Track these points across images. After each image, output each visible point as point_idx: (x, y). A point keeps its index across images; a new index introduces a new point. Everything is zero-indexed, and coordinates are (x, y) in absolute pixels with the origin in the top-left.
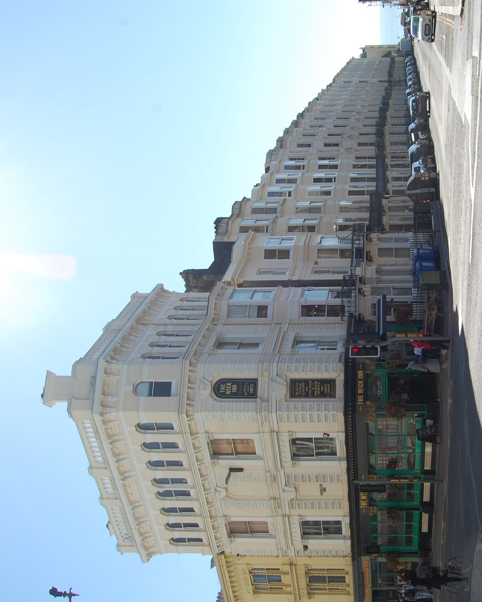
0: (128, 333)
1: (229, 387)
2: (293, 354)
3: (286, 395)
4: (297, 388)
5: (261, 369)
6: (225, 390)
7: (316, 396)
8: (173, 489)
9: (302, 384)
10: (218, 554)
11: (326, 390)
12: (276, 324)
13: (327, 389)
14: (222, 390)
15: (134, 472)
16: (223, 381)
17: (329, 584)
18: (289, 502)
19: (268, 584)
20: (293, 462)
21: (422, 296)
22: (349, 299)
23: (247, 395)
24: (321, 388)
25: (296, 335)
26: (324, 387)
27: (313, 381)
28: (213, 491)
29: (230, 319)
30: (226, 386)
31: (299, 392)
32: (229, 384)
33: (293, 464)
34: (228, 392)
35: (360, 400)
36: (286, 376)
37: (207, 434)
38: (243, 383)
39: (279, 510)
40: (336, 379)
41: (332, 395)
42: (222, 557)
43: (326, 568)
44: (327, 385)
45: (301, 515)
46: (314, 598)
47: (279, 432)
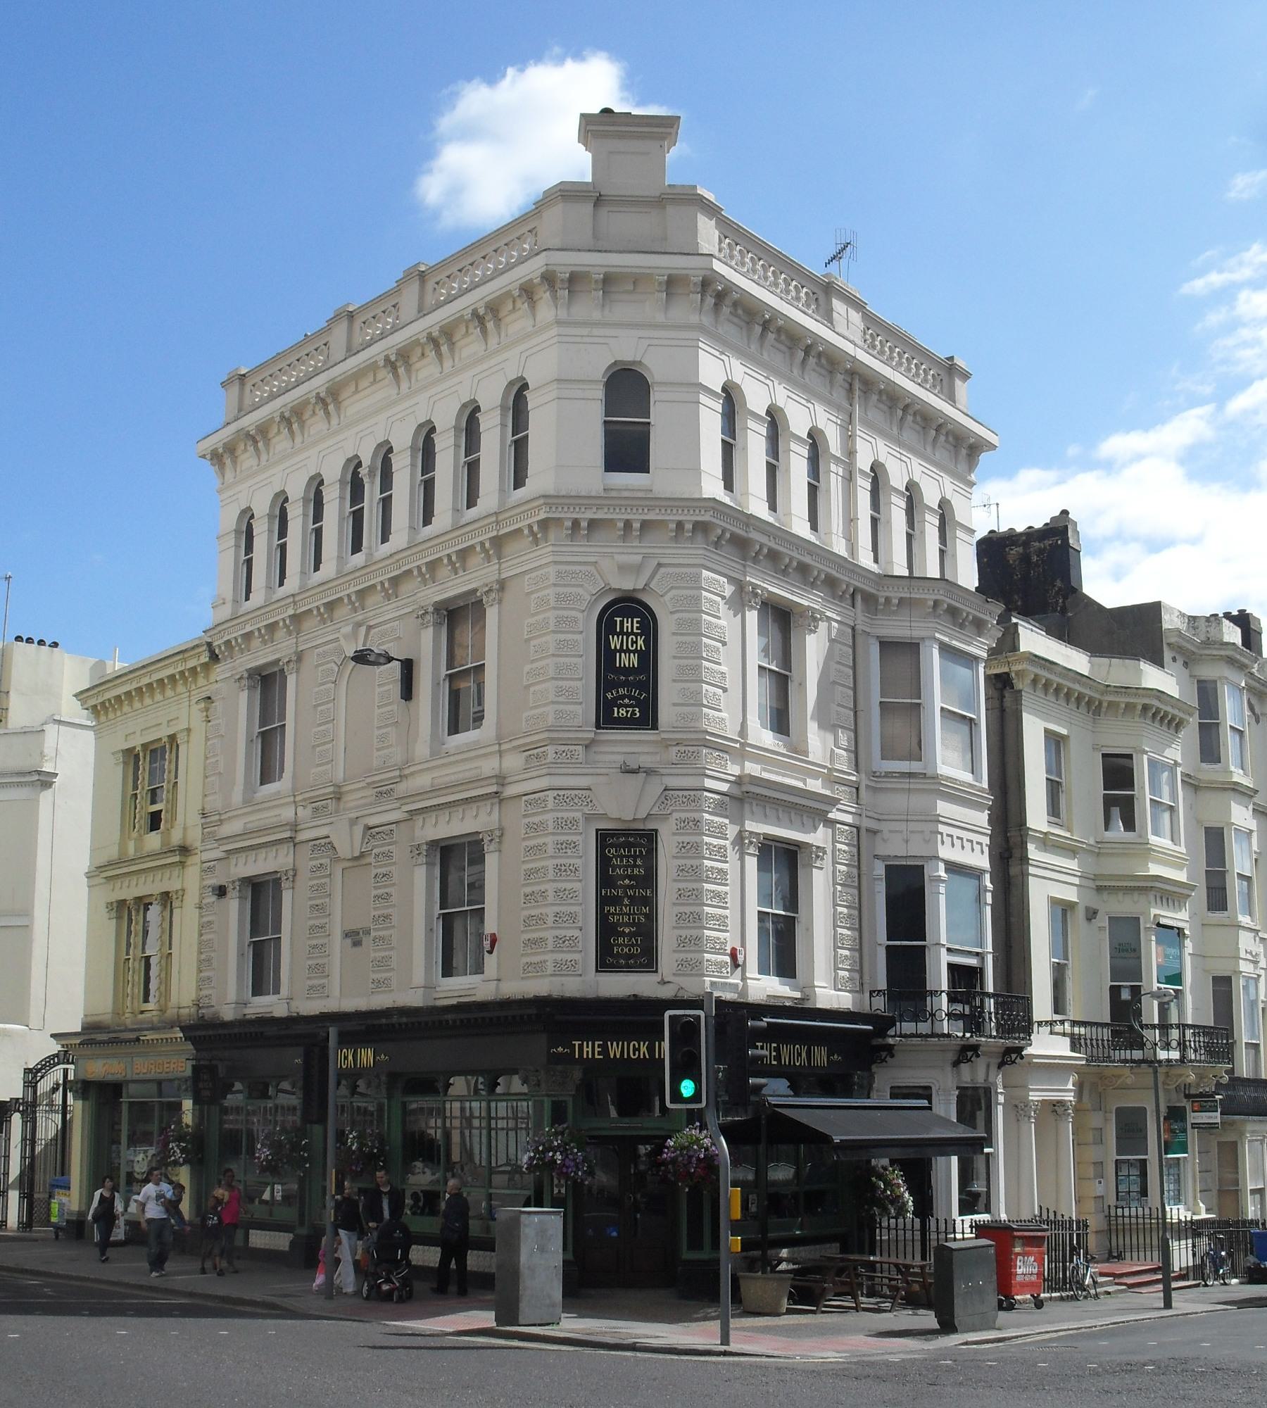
3: (604, 816)
6: (622, 633)
8: (366, 504)
9: (639, 866)
10: (209, 644)
12: (857, 789)
14: (622, 623)
15: (408, 390)
17: (140, 961)
18: (327, 840)
20: (425, 847)
24: (627, 925)
26: (631, 935)
28: (359, 617)
29: (875, 650)
31: (616, 857)
32: (640, 642)
34: (615, 642)
35: (587, 1049)
37: (496, 586)
38: (643, 686)
39: (308, 811)
40: (656, 971)
41: (607, 960)
42: (205, 658)
43: (175, 951)
45: (298, 878)
46: (109, 919)
47: (501, 801)
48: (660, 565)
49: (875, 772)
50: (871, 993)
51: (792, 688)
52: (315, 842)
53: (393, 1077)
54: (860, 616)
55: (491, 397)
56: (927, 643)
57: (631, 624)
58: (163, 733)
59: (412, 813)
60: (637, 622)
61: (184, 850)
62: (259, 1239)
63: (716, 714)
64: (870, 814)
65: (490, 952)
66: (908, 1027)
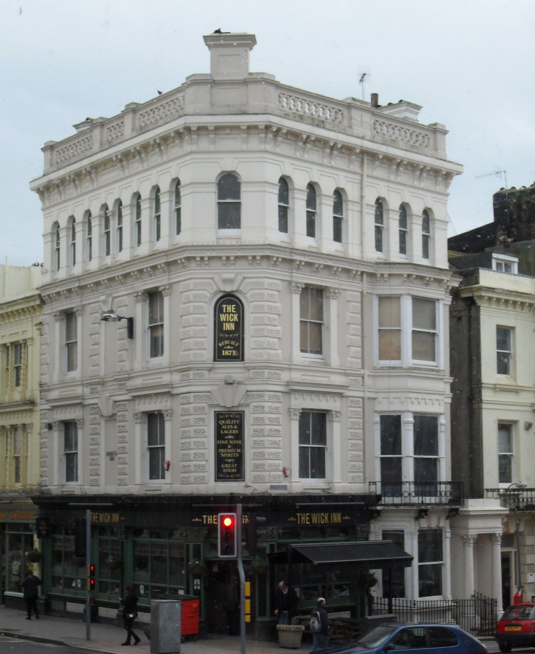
0: (334, 145)
1: (232, 317)
2: (290, 412)
3: (218, 405)
4: (231, 422)
5: (258, 366)
6: (226, 313)
7: (218, 451)
9: (235, 429)
11: (227, 466)
13: (227, 468)
16: (240, 309)
19: (14, 366)
21: (407, 612)
22: (413, 494)
23: (218, 346)
25: (334, 413)
27: (241, 447)
29: (376, 301)
30: (233, 313)
33: (137, 414)
34: (223, 317)
36: (248, 405)
38: (237, 339)
40: (244, 481)
42: (38, 302)
44: (235, 468)
48: (244, 278)
49: (375, 367)
50: (370, 483)
51: (324, 329)
52: (93, 406)
53: (127, 528)
54: (365, 285)
55: (165, 186)
56: (405, 297)
57: (231, 308)
58: (19, 338)
59: (135, 397)
60: (234, 307)
61: (32, 403)
62: (71, 607)
63: (273, 351)
64: (369, 390)
65: (168, 470)
66: (388, 500)
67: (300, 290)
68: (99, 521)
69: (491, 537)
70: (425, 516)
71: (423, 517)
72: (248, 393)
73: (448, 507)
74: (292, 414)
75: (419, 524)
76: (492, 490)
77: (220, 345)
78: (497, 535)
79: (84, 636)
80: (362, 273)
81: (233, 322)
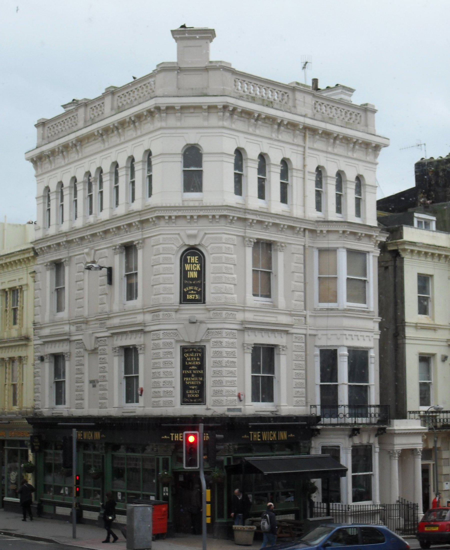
0: (281, 122)
1: (195, 267)
2: (244, 347)
3: (183, 341)
4: (194, 355)
5: (217, 308)
6: (190, 263)
7: (183, 379)
9: (198, 361)
11: (191, 392)
13: (191, 393)
16: (202, 260)
19: (11, 307)
21: (342, 515)
22: (347, 416)
23: (184, 291)
25: (281, 347)
27: (203, 376)
29: (316, 253)
30: (196, 264)
33: (115, 348)
34: (187, 267)
36: (208, 341)
38: (199, 285)
40: (205, 404)
42: (32, 254)
44: (197, 393)
48: (206, 234)
49: (315, 309)
50: (311, 406)
51: (272, 277)
52: (78, 341)
53: (107, 444)
54: (307, 240)
55: (139, 156)
56: (340, 250)
57: (194, 259)
58: (16, 284)
59: (113, 334)
60: (197, 258)
61: (27, 339)
62: (60, 510)
63: (230, 296)
64: (311, 328)
65: (141, 395)
66: (326, 420)
67: (253, 244)
68: (83, 438)
69: (413, 451)
70: (357, 434)
71: (356, 435)
72: (209, 330)
73: (376, 426)
74: (245, 348)
75: (353, 441)
76: (414, 412)
77: (185, 290)
78: (418, 450)
79: (71, 535)
80: (305, 229)
81: (196, 271)
